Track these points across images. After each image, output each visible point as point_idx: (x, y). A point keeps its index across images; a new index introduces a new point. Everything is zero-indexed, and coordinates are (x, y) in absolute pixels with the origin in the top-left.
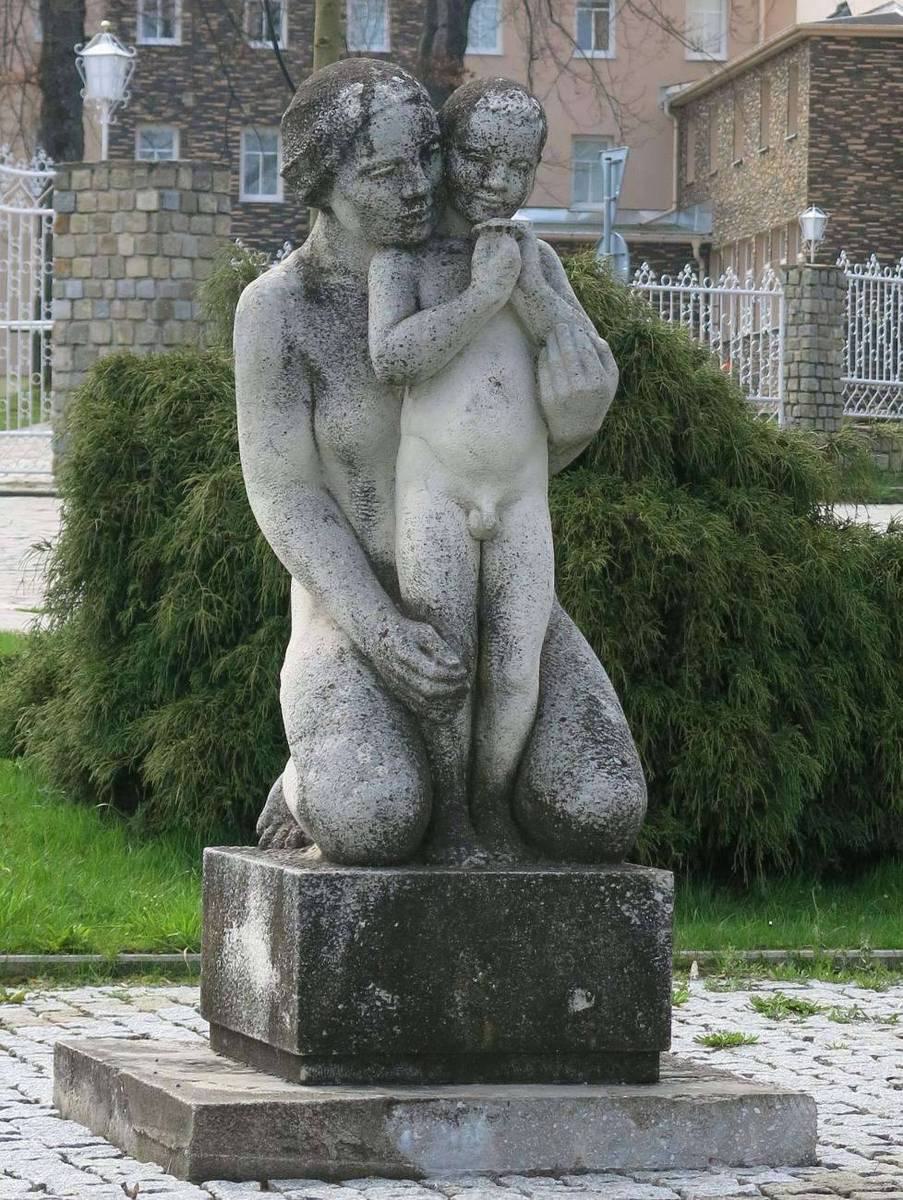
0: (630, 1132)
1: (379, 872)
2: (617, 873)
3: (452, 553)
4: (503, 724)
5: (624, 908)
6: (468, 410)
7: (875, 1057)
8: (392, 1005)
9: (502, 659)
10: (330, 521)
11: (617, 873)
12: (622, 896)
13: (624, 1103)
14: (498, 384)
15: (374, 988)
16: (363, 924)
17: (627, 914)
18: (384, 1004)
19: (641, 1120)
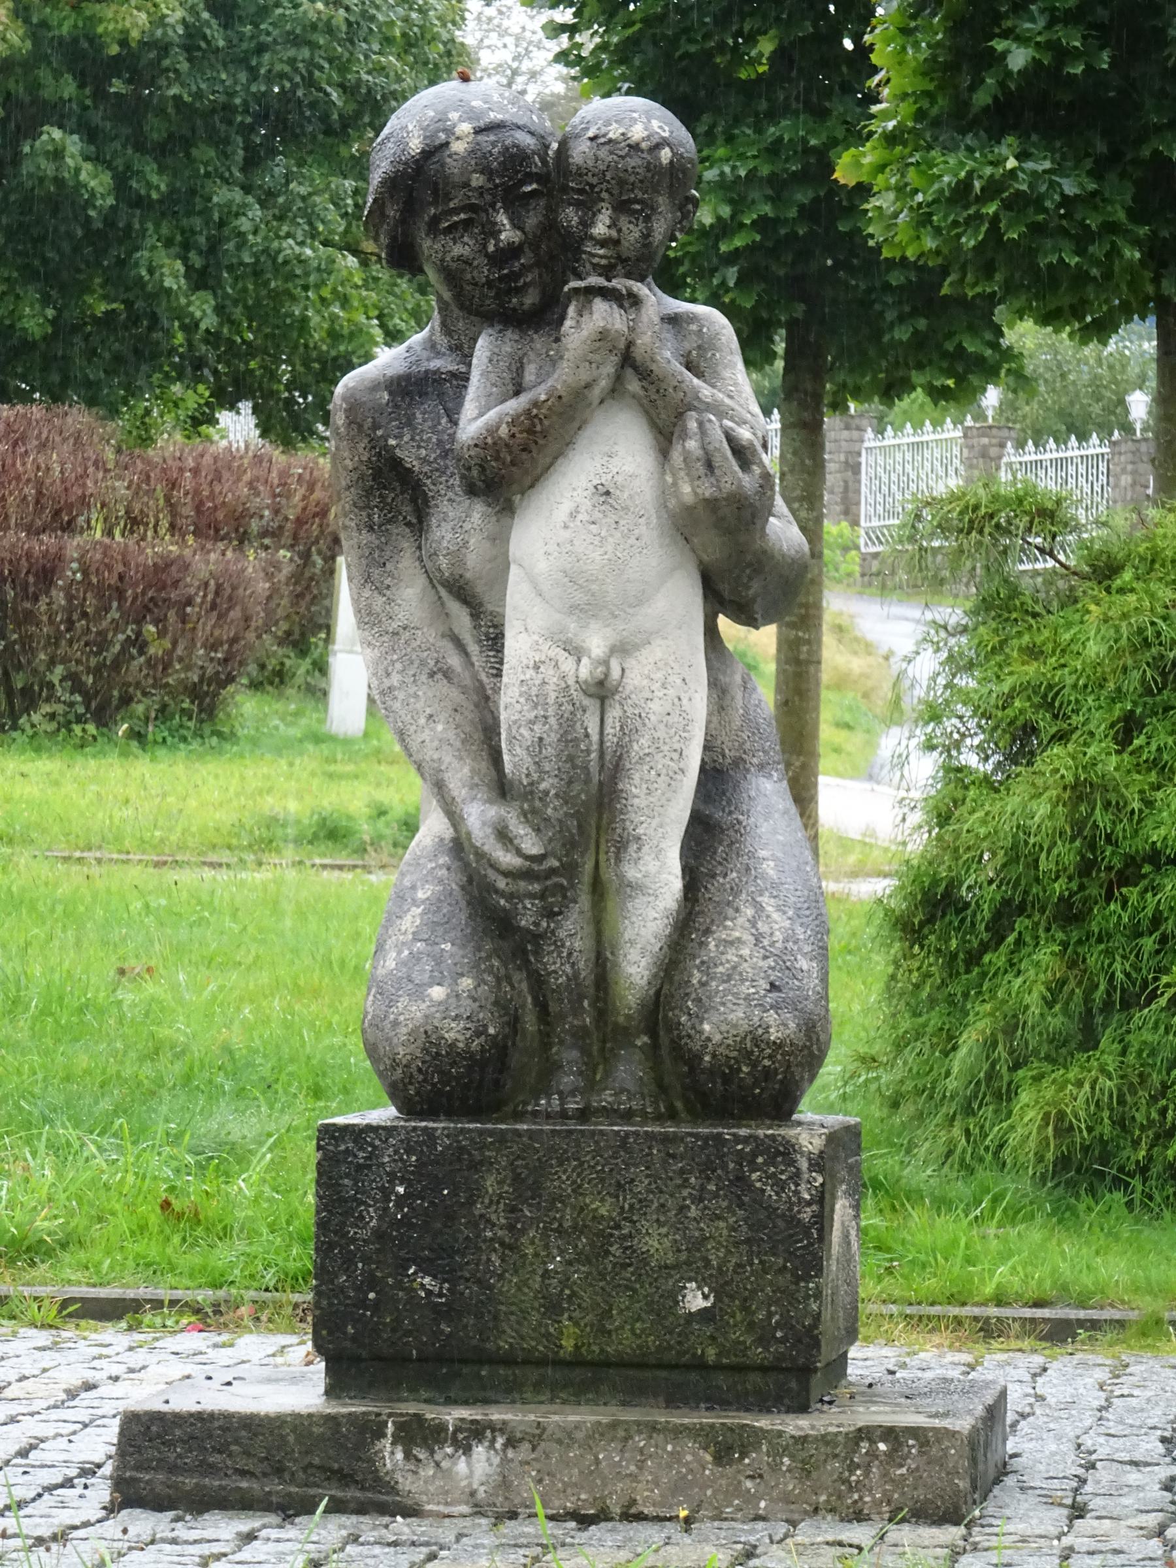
0: (704, 1469)
1: (424, 1124)
2: (743, 1132)
3: (551, 712)
4: (627, 936)
5: (755, 1176)
6: (566, 527)
7: (210, 1378)
8: (440, 1295)
9: (618, 849)
10: (439, 676)
11: (743, 1132)
12: (752, 1162)
13: (695, 1432)
14: (608, 493)
15: (415, 1273)
16: (401, 1190)
17: (758, 1185)
18: (429, 1293)
19: (722, 1456)
